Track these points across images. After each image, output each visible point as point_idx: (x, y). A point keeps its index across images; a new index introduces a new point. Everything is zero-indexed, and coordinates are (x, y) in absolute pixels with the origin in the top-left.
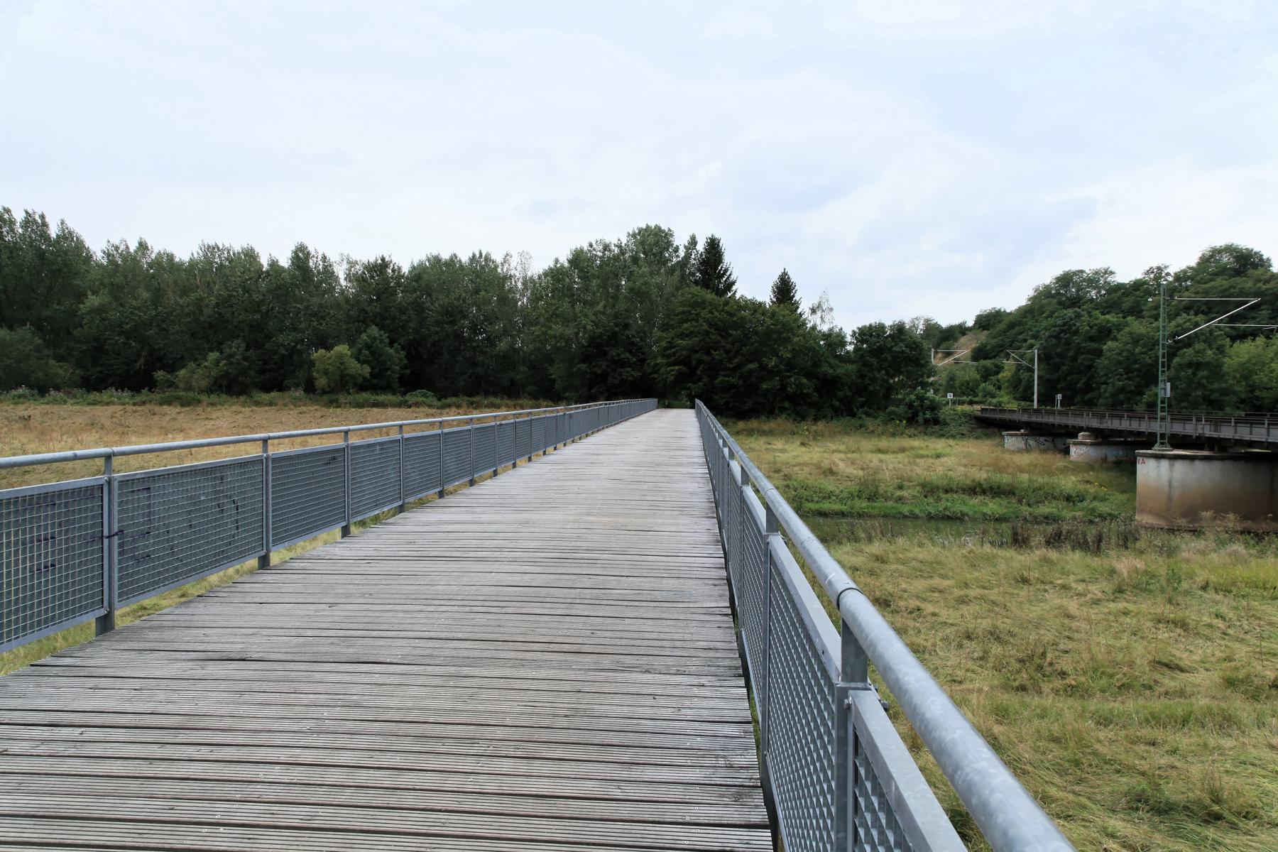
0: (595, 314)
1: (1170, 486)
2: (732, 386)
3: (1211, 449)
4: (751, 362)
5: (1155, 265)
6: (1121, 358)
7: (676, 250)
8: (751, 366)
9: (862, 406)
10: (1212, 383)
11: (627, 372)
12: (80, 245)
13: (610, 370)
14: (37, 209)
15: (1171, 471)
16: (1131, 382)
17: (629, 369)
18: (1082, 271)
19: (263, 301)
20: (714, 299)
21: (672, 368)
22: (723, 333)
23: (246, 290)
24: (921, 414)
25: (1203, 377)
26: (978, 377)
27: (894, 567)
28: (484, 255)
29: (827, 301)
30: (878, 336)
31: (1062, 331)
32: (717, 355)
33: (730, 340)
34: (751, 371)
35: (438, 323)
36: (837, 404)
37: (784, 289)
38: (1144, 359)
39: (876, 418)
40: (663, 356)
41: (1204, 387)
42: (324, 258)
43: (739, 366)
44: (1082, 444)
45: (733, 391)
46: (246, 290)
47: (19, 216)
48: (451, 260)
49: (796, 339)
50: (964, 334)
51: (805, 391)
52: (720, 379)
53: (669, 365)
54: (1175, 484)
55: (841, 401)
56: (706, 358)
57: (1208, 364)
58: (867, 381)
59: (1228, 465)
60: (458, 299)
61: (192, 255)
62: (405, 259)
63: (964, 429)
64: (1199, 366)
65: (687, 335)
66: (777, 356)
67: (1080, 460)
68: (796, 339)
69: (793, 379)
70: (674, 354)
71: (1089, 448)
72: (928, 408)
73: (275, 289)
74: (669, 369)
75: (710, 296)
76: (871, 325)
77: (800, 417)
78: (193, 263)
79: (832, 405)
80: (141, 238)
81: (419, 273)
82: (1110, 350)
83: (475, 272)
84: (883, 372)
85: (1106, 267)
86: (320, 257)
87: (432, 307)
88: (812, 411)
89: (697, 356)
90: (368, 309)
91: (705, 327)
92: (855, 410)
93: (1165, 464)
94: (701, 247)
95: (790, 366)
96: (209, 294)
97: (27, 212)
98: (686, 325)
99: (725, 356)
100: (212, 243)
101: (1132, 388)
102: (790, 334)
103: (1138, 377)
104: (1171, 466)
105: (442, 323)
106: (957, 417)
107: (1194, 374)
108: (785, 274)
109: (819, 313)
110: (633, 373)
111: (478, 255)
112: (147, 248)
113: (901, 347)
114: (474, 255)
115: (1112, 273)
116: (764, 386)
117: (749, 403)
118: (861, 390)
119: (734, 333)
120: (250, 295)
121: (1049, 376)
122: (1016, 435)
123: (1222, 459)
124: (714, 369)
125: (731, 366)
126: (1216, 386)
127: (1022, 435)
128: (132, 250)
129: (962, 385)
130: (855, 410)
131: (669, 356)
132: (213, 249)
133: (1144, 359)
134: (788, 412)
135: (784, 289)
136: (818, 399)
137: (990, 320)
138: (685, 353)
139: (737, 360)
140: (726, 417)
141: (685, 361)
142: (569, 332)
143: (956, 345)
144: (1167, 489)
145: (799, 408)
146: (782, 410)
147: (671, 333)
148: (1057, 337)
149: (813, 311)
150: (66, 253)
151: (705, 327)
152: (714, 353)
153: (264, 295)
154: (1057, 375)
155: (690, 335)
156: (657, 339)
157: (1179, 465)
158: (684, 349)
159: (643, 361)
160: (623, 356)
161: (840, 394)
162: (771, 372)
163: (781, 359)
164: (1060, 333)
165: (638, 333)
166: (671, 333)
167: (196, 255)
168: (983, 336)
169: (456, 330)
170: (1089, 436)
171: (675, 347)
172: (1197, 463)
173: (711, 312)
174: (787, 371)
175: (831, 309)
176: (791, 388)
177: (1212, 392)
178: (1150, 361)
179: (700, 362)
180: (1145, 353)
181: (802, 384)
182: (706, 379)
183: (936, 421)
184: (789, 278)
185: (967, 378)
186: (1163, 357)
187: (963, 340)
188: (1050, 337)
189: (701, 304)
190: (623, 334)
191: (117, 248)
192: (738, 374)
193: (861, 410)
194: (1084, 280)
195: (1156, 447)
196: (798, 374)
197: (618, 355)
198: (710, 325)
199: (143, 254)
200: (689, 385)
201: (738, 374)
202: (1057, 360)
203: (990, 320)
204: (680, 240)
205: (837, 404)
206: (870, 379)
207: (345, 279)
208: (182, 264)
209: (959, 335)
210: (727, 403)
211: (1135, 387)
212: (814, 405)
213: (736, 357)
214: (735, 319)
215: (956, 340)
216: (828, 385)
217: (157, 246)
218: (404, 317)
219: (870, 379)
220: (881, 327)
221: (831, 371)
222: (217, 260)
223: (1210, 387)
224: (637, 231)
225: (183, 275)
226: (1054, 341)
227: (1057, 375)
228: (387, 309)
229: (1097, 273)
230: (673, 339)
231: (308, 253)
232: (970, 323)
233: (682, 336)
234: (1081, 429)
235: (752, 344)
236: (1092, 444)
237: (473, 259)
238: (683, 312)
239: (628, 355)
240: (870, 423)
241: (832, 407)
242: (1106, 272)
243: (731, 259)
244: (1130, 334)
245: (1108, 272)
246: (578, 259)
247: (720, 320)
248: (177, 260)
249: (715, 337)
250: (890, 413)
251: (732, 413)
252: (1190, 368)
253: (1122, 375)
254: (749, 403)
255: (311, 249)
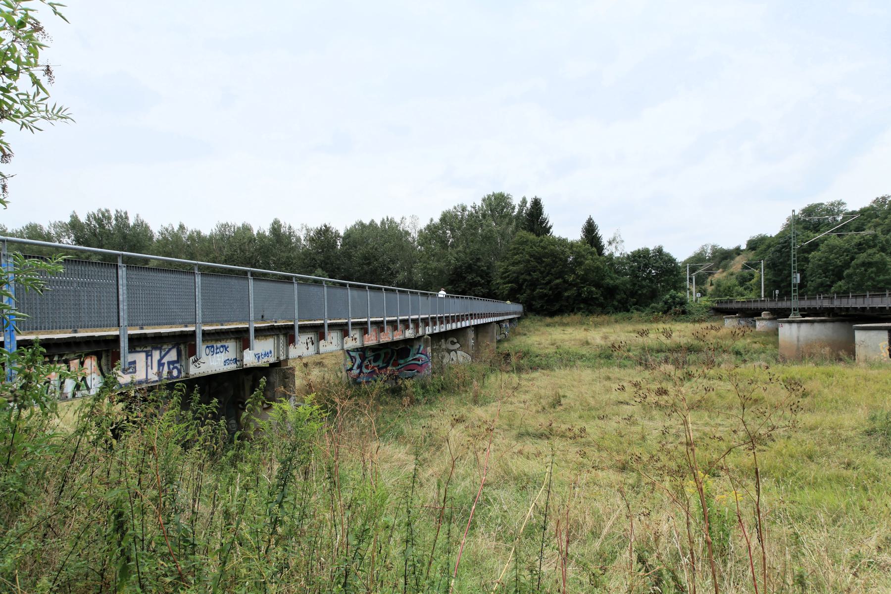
0: (457, 253)
1: (798, 341)
2: (546, 295)
3: (829, 316)
4: (557, 278)
5: (880, 196)
6: (820, 263)
7: (514, 208)
8: (558, 281)
9: (634, 305)
10: (879, 276)
11: (479, 290)
12: (147, 228)
13: (467, 289)
14: (123, 208)
15: (799, 331)
16: (827, 279)
17: (479, 288)
18: (822, 204)
19: (252, 257)
20: (534, 239)
21: (507, 285)
22: (539, 261)
23: (242, 251)
24: (673, 308)
25: (872, 272)
26: (737, 283)
27: (735, 437)
28: (389, 219)
29: (620, 236)
30: (644, 257)
31: (783, 247)
32: (535, 275)
33: (543, 265)
34: (557, 285)
35: (360, 265)
36: (616, 303)
37: (590, 229)
38: (836, 262)
39: (643, 312)
40: (501, 278)
41: (873, 279)
42: (290, 227)
43: (549, 282)
44: (763, 319)
45: (546, 298)
46: (242, 251)
47: (113, 214)
48: (370, 224)
49: (587, 262)
50: (739, 254)
51: (594, 296)
52: (538, 290)
53: (504, 283)
54: (801, 339)
55: (619, 302)
56: (528, 277)
57: (876, 262)
58: (637, 287)
59: (837, 325)
60: (372, 249)
61: (212, 230)
62: (341, 225)
63: (703, 317)
64: (869, 265)
65: (517, 263)
66: (574, 273)
67: (762, 330)
68: (587, 262)
69: (585, 289)
70: (508, 275)
71: (768, 322)
72: (678, 304)
73: (260, 249)
74: (504, 286)
75: (532, 237)
76: (639, 250)
77: (591, 312)
78: (211, 237)
79: (613, 304)
80: (181, 223)
81: (432, 233)
82: (814, 258)
83: (385, 231)
84: (648, 281)
85: (839, 199)
86: (287, 227)
87: (356, 255)
88: (599, 309)
89: (522, 277)
90: (316, 258)
91: (527, 257)
92: (629, 307)
93: (795, 326)
94: (528, 205)
95: (584, 279)
96: (220, 254)
97: (117, 211)
98: (516, 257)
99: (540, 275)
100: (224, 222)
101: (828, 283)
102: (582, 259)
103: (833, 275)
104: (799, 327)
105: (362, 265)
106: (700, 309)
107: (866, 270)
108: (590, 219)
109: (614, 245)
110: (482, 290)
111: (386, 220)
112: (184, 228)
113: (660, 263)
114: (383, 220)
115: (843, 204)
116: (566, 294)
117: (557, 306)
118: (633, 294)
119: (546, 260)
120: (245, 254)
121: (774, 278)
122: (732, 318)
123: (833, 321)
124: (534, 284)
125: (545, 282)
126: (881, 277)
127: (736, 317)
128: (175, 230)
129: (726, 289)
130: (629, 307)
131: (505, 278)
132: (225, 226)
133: (836, 262)
134: (583, 311)
135: (590, 229)
136: (603, 301)
137: (757, 243)
138: (515, 275)
139: (548, 278)
140: (542, 315)
141: (515, 281)
142: (442, 264)
143: (732, 262)
144: (796, 342)
145: (590, 308)
146: (579, 309)
147: (506, 263)
148: (780, 251)
149: (610, 243)
150: (138, 234)
151: (527, 257)
152: (533, 274)
153: (253, 253)
154: (781, 277)
155: (519, 263)
156: (499, 266)
157: (804, 326)
158: (514, 273)
159: (489, 282)
160: (475, 279)
161: (618, 297)
162: (570, 284)
163: (578, 276)
164: (782, 248)
165: (485, 263)
166: (506, 263)
167: (214, 231)
168: (751, 255)
169: (371, 269)
170: (768, 314)
171: (509, 271)
172: (816, 325)
173: (531, 247)
174: (582, 283)
175: (622, 241)
176: (585, 294)
177: (879, 282)
178: (840, 264)
179: (525, 280)
180: (837, 258)
181: (592, 292)
182: (528, 291)
183: (684, 312)
184: (593, 222)
185: (729, 284)
186: (794, 257)
187: (738, 258)
188: (775, 251)
189: (524, 242)
190: (476, 265)
191: (167, 230)
192: (548, 287)
193: (633, 307)
194: (823, 211)
195: (791, 316)
196: (589, 285)
197: (473, 279)
198: (531, 256)
199: (182, 232)
200: (518, 296)
201: (548, 287)
202: (780, 267)
203: (757, 243)
204: (516, 201)
205: (616, 303)
206: (639, 286)
207: (304, 240)
208: (261, 236)
209: (734, 255)
210: (542, 306)
211: (830, 282)
212: (601, 305)
213: (547, 276)
214: (546, 251)
215: (733, 258)
216: (611, 292)
217: (191, 227)
218: (338, 262)
219: (639, 286)
220: (647, 251)
221: (611, 282)
222: (227, 233)
223: (877, 278)
224: (486, 197)
225: (207, 244)
226: (778, 254)
227: (781, 277)
228: (328, 258)
229: (832, 204)
230: (508, 266)
231: (281, 225)
232: (744, 247)
233: (514, 264)
234: (764, 310)
235: (558, 267)
236: (769, 319)
237: (383, 223)
238: (515, 249)
239: (479, 278)
240: (636, 314)
241: (613, 305)
242: (839, 204)
243: (549, 213)
244: (828, 245)
245: (840, 203)
246: (446, 218)
247: (537, 252)
248: (202, 234)
249: (534, 263)
250: (652, 308)
251: (546, 313)
252: (864, 266)
253: (821, 274)
254: (557, 306)
255: (282, 222)
